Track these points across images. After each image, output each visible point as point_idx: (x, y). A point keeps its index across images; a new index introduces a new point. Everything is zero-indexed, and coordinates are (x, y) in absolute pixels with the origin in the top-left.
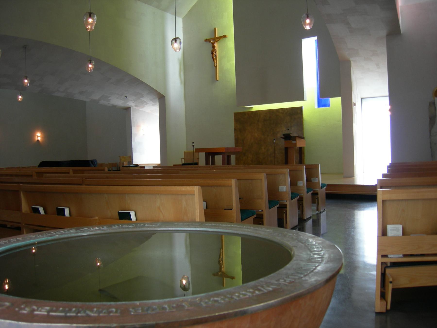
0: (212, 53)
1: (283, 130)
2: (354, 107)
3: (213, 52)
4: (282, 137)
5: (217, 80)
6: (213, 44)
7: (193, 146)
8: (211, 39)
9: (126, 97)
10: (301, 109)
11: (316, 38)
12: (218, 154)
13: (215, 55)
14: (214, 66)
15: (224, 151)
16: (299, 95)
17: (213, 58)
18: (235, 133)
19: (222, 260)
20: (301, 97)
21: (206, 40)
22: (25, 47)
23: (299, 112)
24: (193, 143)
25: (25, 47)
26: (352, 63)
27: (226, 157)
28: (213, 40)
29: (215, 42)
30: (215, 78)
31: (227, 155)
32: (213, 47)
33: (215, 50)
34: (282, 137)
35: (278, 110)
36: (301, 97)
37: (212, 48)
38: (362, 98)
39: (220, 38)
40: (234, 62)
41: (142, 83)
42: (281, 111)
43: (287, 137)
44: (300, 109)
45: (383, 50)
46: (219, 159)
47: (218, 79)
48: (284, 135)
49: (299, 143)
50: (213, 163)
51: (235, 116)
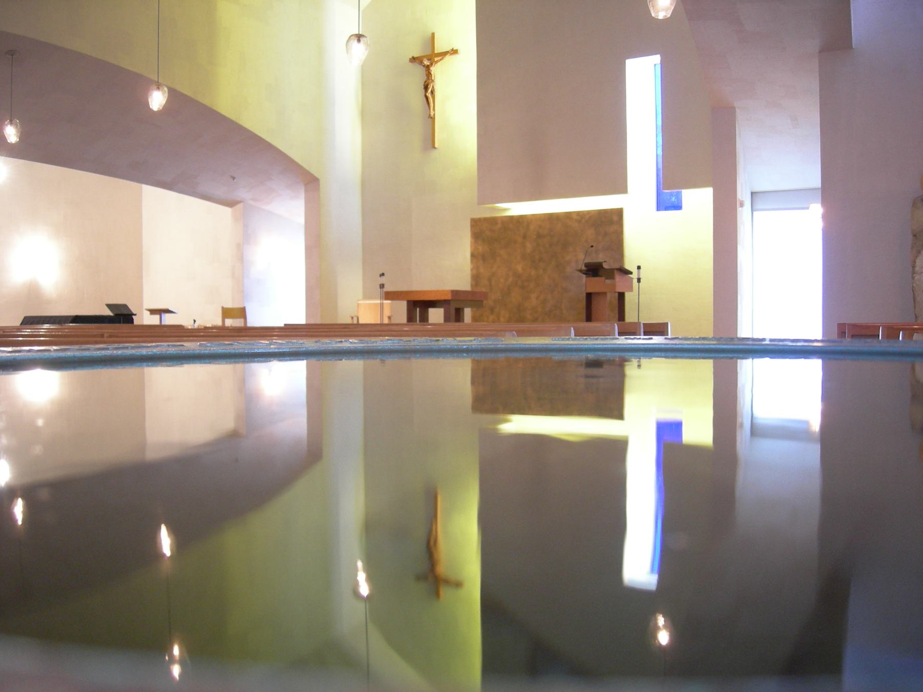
0: (426, 88)
1: (580, 258)
2: (739, 209)
4: (581, 271)
5: (434, 147)
6: (428, 68)
7: (382, 286)
8: (424, 57)
9: (234, 178)
11: (656, 59)
12: (433, 304)
13: (432, 92)
14: (430, 117)
15: (449, 297)
17: (427, 98)
18: (472, 262)
20: (621, 188)
21: (413, 60)
22: (12, 53)
23: (615, 218)
24: (383, 274)
25: (12, 53)
26: (740, 116)
27: (453, 312)
28: (427, 60)
29: (432, 64)
30: (430, 142)
31: (454, 306)
32: (429, 74)
33: (433, 81)
34: (581, 271)
35: (568, 215)
36: (621, 188)
37: (425, 78)
38: (752, 193)
39: (444, 54)
41: (270, 147)
42: (575, 217)
43: (593, 270)
45: (814, 84)
48: (587, 265)
49: (619, 283)
50: (424, 319)
51: (472, 226)
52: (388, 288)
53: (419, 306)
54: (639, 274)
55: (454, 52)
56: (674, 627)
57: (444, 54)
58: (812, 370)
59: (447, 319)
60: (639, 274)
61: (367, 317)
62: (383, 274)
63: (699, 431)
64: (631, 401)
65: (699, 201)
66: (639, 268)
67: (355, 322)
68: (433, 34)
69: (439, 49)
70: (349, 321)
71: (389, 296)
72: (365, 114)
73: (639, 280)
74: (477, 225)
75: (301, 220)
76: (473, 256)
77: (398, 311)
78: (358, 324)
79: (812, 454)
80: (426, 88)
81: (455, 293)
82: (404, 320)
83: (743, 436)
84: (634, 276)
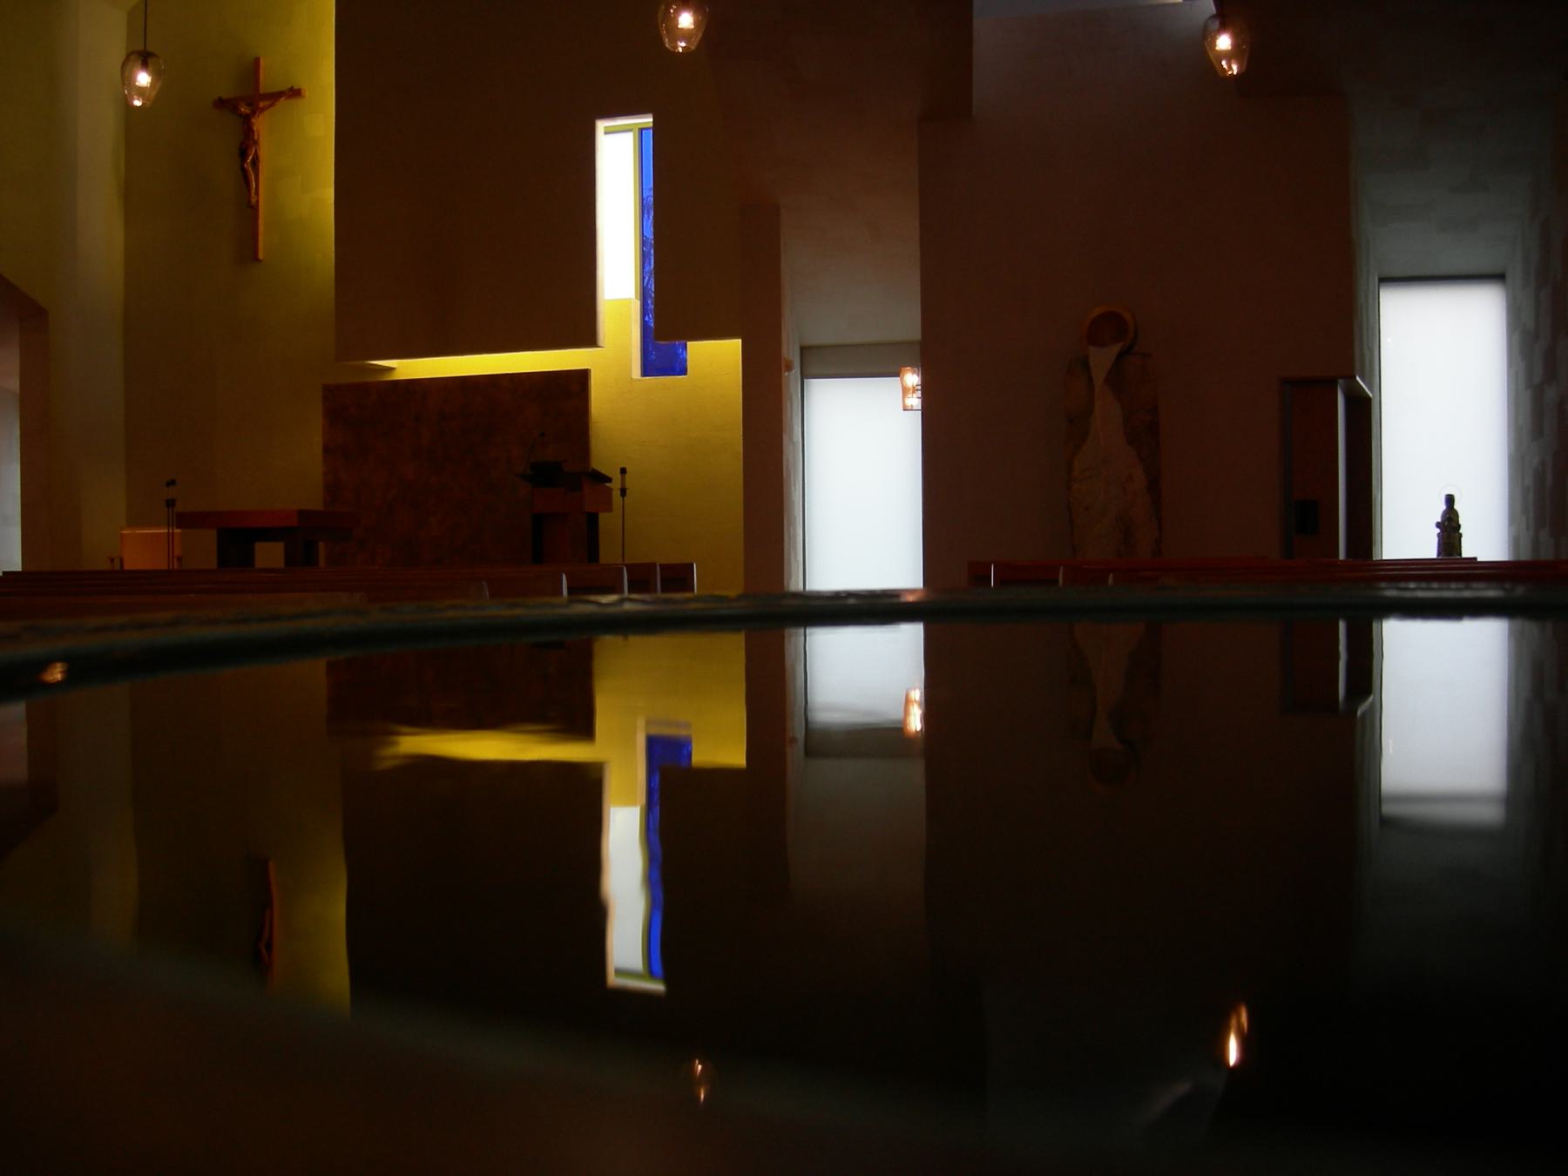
3: (246, 145)
5: (256, 259)
7: (170, 503)
10: (582, 377)
11: (647, 120)
13: (255, 162)
16: (579, 326)
17: (244, 172)
19: (269, 946)
21: (221, 103)
24: (171, 483)
28: (247, 101)
29: (254, 113)
30: (247, 249)
31: (302, 535)
33: (256, 143)
38: (802, 349)
39: (275, 97)
40: (330, 193)
41: (819, 347)
44: (579, 380)
46: (270, 555)
47: (261, 256)
50: (247, 560)
52: (179, 508)
53: (237, 538)
54: (623, 481)
55: (1450, 500)
56: (693, 1069)
57: (275, 97)
58: (908, 639)
59: (290, 559)
60: (623, 481)
61: (136, 560)
62: (171, 483)
63: (722, 746)
64: (603, 721)
65: (717, 359)
66: (623, 471)
67: (117, 567)
68: (257, 61)
69: (267, 84)
70: (106, 566)
71: (186, 520)
72: (132, 197)
73: (623, 492)
74: (332, 395)
75: (14, 384)
76: (326, 449)
77: (203, 549)
78: (122, 571)
79: (914, 774)
80: (243, 154)
81: (304, 514)
82: (212, 563)
83: (795, 753)
84: (615, 485)
